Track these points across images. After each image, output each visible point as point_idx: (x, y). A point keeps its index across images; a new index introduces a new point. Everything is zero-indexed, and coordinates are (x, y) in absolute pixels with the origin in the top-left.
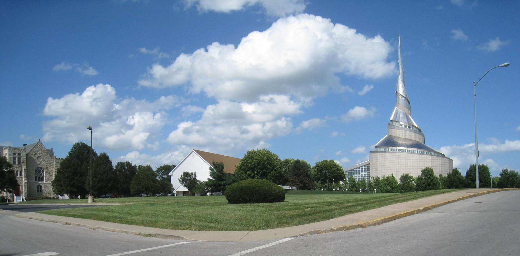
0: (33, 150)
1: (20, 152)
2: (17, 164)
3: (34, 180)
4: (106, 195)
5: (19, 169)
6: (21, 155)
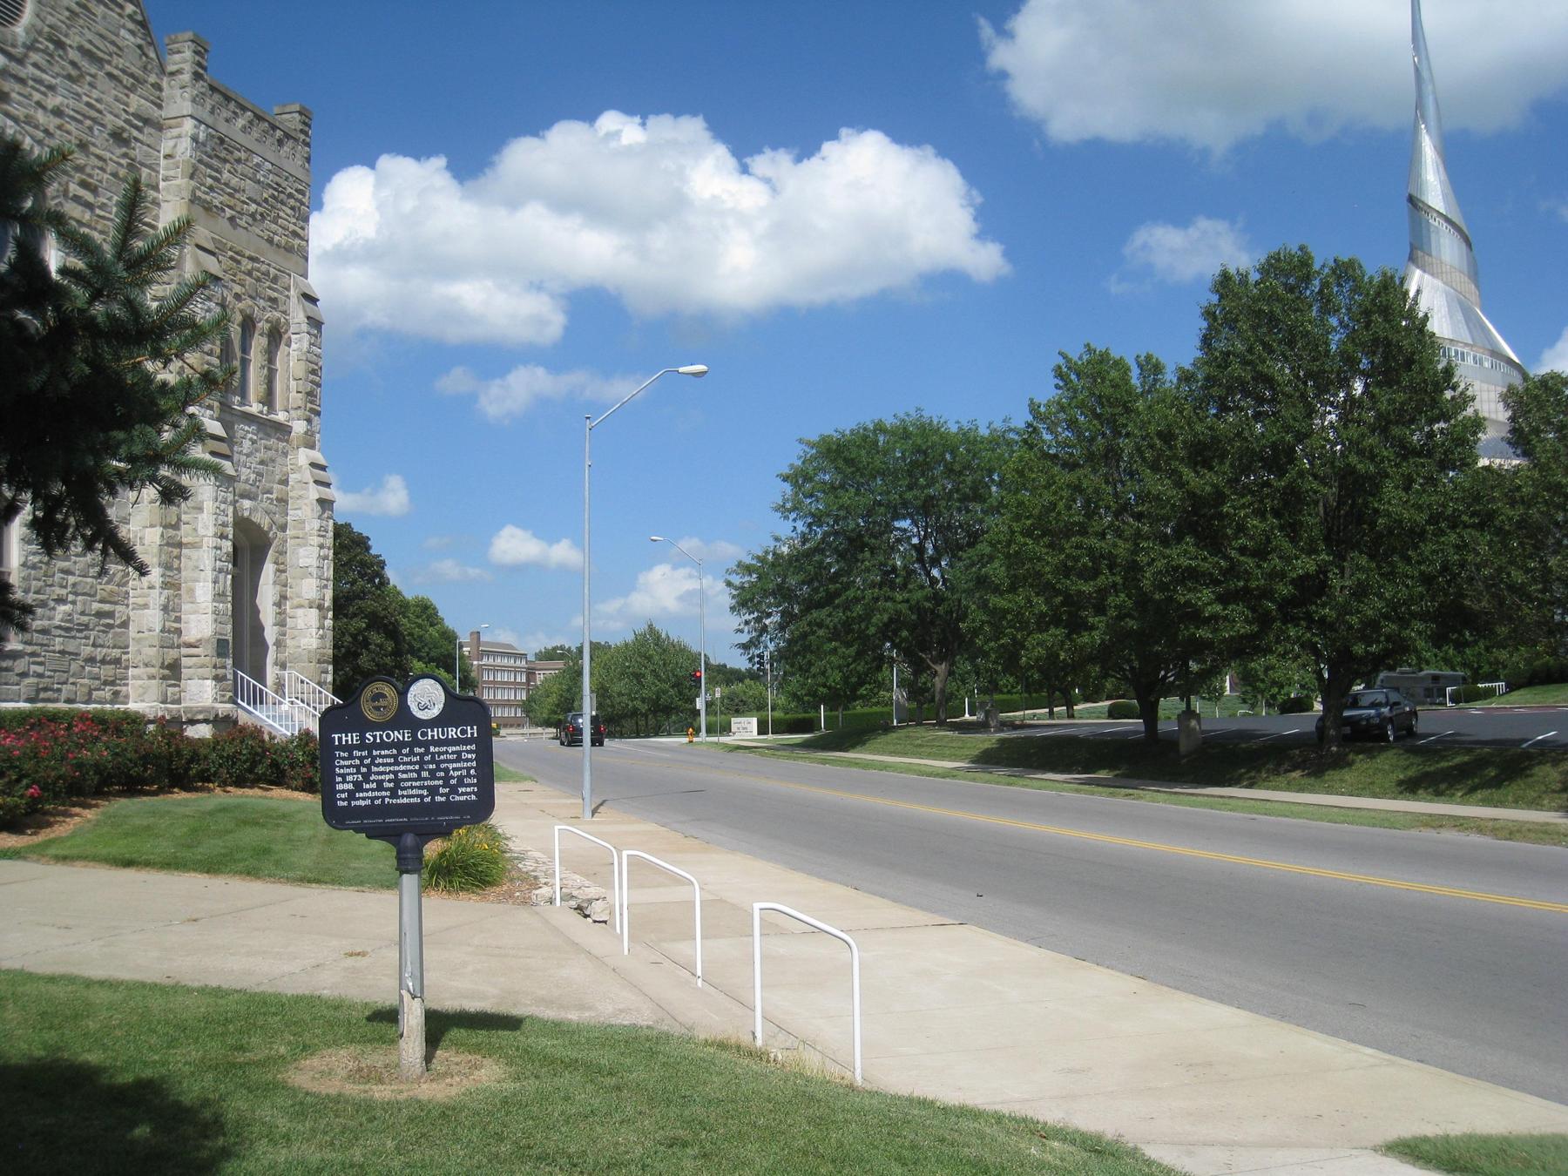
4: (383, 801)
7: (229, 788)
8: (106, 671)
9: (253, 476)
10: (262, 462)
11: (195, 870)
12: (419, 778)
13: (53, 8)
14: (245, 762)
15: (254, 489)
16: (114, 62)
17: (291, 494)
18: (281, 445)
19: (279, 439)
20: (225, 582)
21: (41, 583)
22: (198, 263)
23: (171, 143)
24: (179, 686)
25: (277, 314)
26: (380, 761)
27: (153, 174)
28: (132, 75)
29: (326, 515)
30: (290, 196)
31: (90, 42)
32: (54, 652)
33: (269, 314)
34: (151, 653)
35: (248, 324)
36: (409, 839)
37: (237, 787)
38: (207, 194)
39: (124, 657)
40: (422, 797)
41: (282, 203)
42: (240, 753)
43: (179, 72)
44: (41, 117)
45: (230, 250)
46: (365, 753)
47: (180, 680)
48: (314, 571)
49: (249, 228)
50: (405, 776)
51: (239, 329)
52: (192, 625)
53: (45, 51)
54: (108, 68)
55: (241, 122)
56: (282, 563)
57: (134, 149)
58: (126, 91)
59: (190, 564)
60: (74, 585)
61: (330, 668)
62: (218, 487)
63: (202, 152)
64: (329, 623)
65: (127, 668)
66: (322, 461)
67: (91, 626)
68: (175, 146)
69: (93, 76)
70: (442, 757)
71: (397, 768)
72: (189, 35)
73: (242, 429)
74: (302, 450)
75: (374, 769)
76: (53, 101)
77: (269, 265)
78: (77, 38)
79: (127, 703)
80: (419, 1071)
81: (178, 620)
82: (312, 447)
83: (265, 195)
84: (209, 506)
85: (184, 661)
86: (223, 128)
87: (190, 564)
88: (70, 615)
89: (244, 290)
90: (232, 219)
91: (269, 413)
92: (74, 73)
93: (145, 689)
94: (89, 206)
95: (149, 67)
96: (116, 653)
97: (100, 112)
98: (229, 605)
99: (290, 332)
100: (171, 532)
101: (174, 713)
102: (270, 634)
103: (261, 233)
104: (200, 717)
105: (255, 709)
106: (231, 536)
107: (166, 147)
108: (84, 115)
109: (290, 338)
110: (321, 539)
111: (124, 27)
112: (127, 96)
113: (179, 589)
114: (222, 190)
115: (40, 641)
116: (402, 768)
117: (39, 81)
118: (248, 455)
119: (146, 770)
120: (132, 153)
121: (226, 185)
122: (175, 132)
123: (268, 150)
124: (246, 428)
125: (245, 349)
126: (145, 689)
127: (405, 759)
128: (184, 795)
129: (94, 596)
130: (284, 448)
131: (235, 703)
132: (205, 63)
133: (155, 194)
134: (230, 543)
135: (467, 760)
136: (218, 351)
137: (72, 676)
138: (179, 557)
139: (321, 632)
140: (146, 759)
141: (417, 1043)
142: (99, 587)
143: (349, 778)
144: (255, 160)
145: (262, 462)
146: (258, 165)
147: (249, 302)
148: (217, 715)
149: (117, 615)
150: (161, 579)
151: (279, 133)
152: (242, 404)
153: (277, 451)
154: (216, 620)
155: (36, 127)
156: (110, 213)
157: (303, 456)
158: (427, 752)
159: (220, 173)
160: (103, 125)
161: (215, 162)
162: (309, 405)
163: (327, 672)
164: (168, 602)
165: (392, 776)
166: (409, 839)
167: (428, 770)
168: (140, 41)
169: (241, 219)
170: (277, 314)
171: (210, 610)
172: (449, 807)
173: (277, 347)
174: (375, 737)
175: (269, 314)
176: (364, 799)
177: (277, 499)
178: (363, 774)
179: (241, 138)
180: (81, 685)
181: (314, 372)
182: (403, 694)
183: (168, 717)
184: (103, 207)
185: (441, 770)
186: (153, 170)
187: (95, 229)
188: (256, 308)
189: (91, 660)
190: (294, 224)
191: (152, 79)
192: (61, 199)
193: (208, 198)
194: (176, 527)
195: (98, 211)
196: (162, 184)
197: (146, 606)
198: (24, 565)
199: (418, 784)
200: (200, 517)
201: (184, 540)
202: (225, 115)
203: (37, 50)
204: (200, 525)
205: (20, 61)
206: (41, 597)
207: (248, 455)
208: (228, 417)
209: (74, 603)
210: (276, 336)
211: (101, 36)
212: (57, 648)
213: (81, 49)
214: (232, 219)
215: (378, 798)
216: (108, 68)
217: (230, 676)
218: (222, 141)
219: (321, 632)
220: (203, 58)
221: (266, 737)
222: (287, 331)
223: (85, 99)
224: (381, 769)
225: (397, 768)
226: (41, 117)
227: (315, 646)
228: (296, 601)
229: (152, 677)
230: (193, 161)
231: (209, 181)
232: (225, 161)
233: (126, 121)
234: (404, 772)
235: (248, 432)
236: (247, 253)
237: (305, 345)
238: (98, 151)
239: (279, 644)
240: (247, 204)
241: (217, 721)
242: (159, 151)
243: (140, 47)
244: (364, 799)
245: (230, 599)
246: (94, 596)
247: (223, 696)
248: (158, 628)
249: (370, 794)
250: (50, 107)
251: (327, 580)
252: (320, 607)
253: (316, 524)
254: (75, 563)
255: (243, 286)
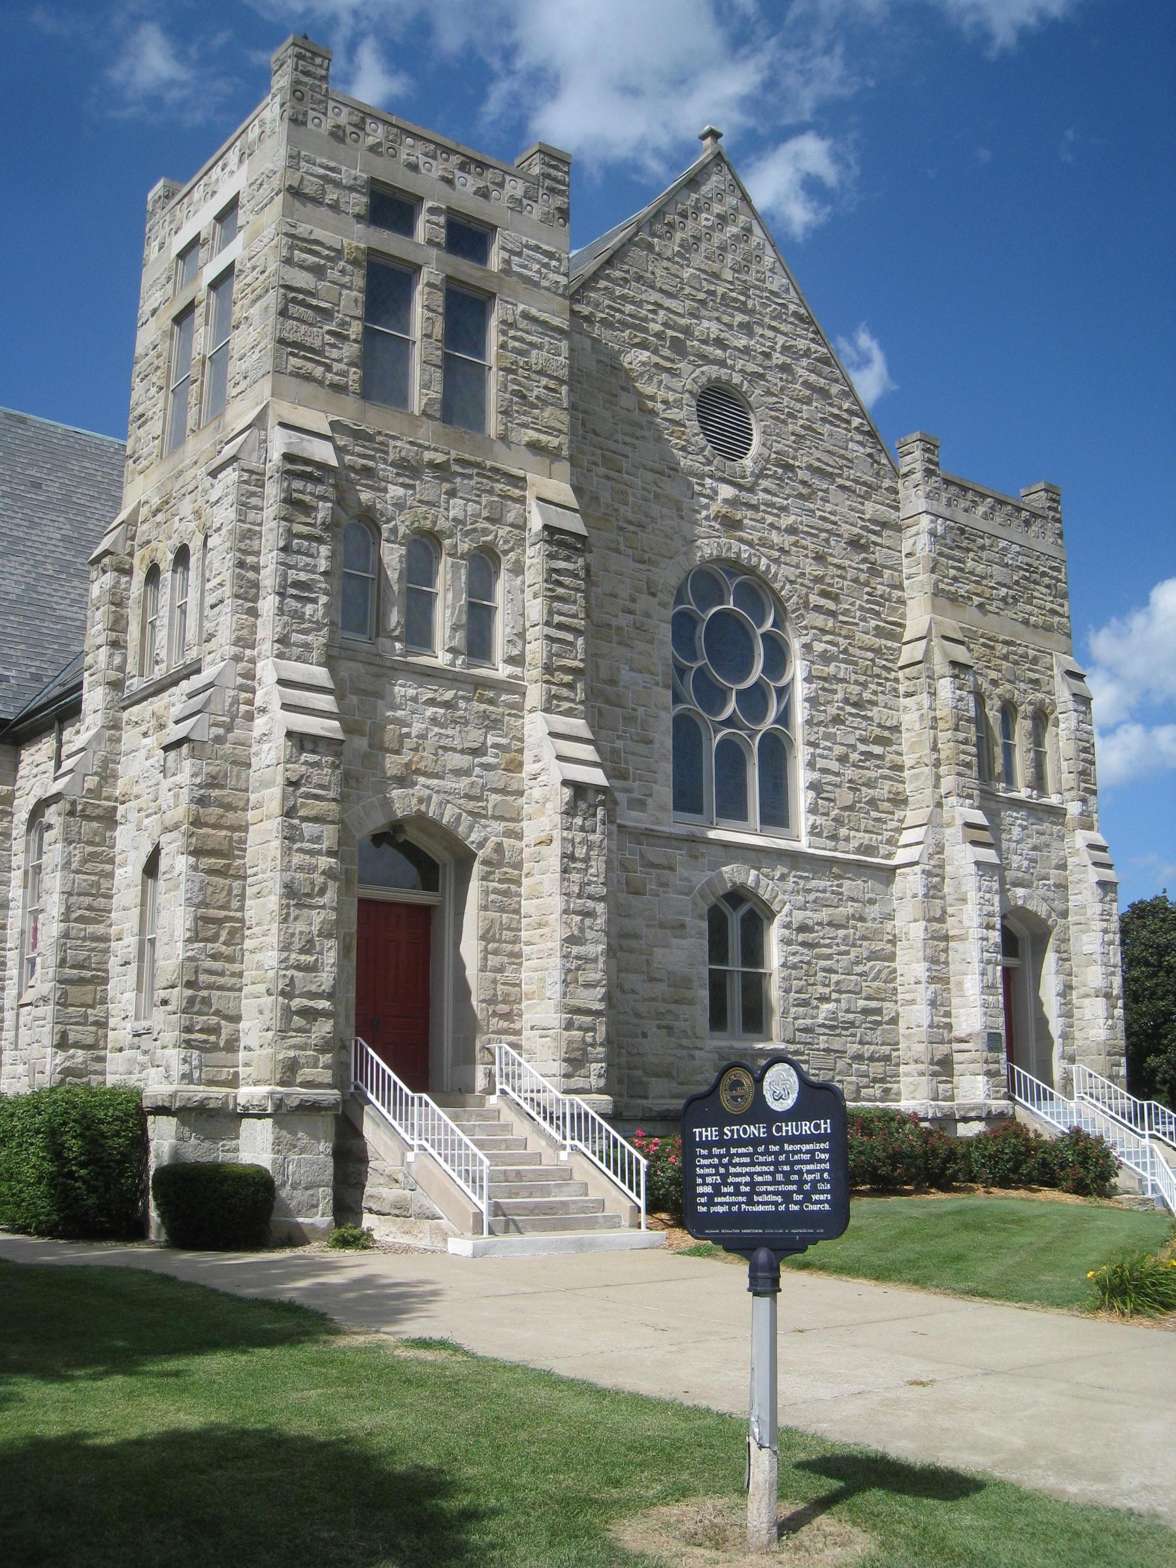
0: (636, 253)
1: (484, 193)
2: (417, 402)
3: (665, 792)
4: (740, 1208)
5: (457, 508)
6: (495, 260)
7: (992, 1189)
8: (876, 1069)
9: (1026, 863)
10: (1035, 848)
11: (865, 1276)
12: (774, 1182)
13: (778, 435)
14: (1008, 1161)
15: (1027, 876)
16: (845, 474)
17: (1070, 879)
18: (1056, 828)
19: (1052, 823)
20: (995, 974)
21: (803, 983)
22: (945, 654)
23: (912, 541)
24: (951, 1082)
25: (1040, 696)
26: (736, 1160)
27: (896, 574)
28: (865, 484)
29: (1108, 898)
30: (1044, 574)
31: (818, 460)
32: (818, 1050)
33: (1031, 697)
34: (920, 1049)
35: (1009, 710)
36: (762, 1255)
37: (1001, 1187)
38: (952, 585)
39: (895, 1054)
40: (776, 1204)
41: (1036, 583)
42: (1002, 1152)
43: (911, 472)
44: (775, 537)
45: (982, 637)
46: (723, 1151)
47: (952, 1076)
48: (1098, 957)
49: (1002, 613)
50: (760, 1179)
51: (999, 715)
52: (963, 1019)
53: (774, 476)
54: (839, 481)
55: (981, 510)
56: (1065, 952)
57: (873, 553)
58: (860, 500)
59: (958, 957)
60: (838, 983)
61: (1123, 1060)
62: (981, 876)
63: (941, 545)
64: (1119, 1012)
65: (898, 1065)
66: (1102, 842)
67: (857, 1023)
68: (914, 544)
69: (826, 491)
70: (796, 1157)
71: (753, 1169)
72: (917, 435)
73: (1009, 816)
74: (1078, 831)
75: (732, 1170)
76: (786, 521)
77: (1026, 647)
78: (805, 459)
79: (898, 1101)
80: (765, 1538)
81: (948, 1014)
82: (1090, 828)
83: (1015, 578)
84: (973, 896)
85: (957, 1057)
86: (962, 518)
87: (958, 957)
88: (833, 1013)
89: (1000, 675)
90: (981, 606)
91: (1039, 797)
92: (805, 491)
93: (916, 1086)
94: (832, 614)
95: (882, 473)
96: (886, 1049)
97: (835, 523)
98: (1001, 998)
99: (1056, 714)
100: (936, 926)
101: (946, 1110)
102: (1055, 1027)
103: (1015, 616)
104: (973, 1114)
105: (1039, 1109)
106: (998, 926)
107: (906, 547)
108: (817, 529)
109: (1057, 719)
110: (1105, 924)
111: (852, 440)
112: (863, 504)
113: (948, 983)
114: (967, 579)
115: (803, 1040)
116: (758, 1169)
117: (772, 505)
118: (1018, 842)
119: (894, 1170)
120: (872, 557)
121: (972, 573)
122: (913, 530)
123: (1016, 533)
124: (1015, 814)
125: (1008, 733)
126: (916, 1086)
127: (762, 1159)
128: (942, 1196)
129: (859, 993)
130: (1059, 831)
131: (1012, 1099)
132: (936, 459)
133: (900, 593)
134: (997, 933)
135: (821, 1161)
136: (974, 739)
137: (838, 1074)
138: (946, 950)
139: (1110, 1022)
140: (895, 1158)
141: (763, 1503)
142: (864, 984)
143: (709, 1180)
144: (1001, 545)
145: (1035, 848)
146: (1003, 549)
147: (1008, 686)
148: (990, 1112)
149: (885, 1012)
150: (927, 974)
151: (1024, 514)
152: (1007, 790)
153: (1051, 835)
154: (985, 1014)
155: (771, 547)
156: (854, 618)
157: (1081, 838)
158: (782, 1151)
159: (964, 563)
160: (839, 535)
161: (956, 553)
162: (1083, 785)
163: (1119, 1065)
164: (936, 997)
165: (748, 1179)
166: (762, 1255)
167: (782, 1172)
168: (869, 450)
169: (991, 605)
170: (1040, 696)
171: (978, 1003)
172: (803, 1218)
173: (1045, 728)
174: (732, 1131)
175: (1031, 697)
176: (722, 1204)
177: (1055, 885)
178: (721, 1175)
179: (983, 525)
180: (849, 1083)
181: (1085, 750)
182: (759, 1081)
183: (939, 1115)
184: (846, 612)
185: (795, 1173)
186: (896, 570)
187: (840, 635)
188: (1016, 692)
189: (858, 1058)
190: (1052, 602)
191: (887, 483)
192: (802, 611)
193: (953, 589)
194: (941, 920)
195: (841, 618)
196: (906, 583)
197: (913, 1002)
198: (784, 965)
199: (771, 1188)
200: (964, 907)
201: (951, 933)
202: (963, 505)
203: (767, 476)
204: (965, 917)
205: (751, 490)
206: (803, 996)
207: (1018, 842)
208: (993, 805)
209: (838, 1001)
210: (1041, 718)
211: (829, 452)
212: (822, 1046)
213: (809, 467)
214: (981, 606)
215: (734, 1204)
216: (839, 481)
217: (1004, 1072)
218: (962, 531)
219: (1110, 1022)
220: (933, 454)
221: (1032, 1135)
222: (1053, 712)
223: (818, 513)
224: (738, 1170)
225: (753, 1169)
226: (775, 537)
227: (1103, 1038)
228: (1082, 990)
229: (922, 1074)
230: (933, 555)
231: (952, 572)
232: (968, 550)
233: (862, 528)
234: (760, 1174)
235: (1017, 818)
236: (1001, 638)
237: (1073, 724)
238: (835, 561)
239: (1065, 1036)
240: (996, 589)
241: (989, 1118)
242: (900, 552)
243: (870, 455)
244: (722, 1204)
245: (1001, 991)
246: (859, 993)
247: (997, 1092)
248: (926, 1022)
249: (727, 1199)
250: (783, 527)
251: (1115, 966)
252: (1108, 996)
253: (1098, 908)
254: (838, 961)
255: (999, 671)
